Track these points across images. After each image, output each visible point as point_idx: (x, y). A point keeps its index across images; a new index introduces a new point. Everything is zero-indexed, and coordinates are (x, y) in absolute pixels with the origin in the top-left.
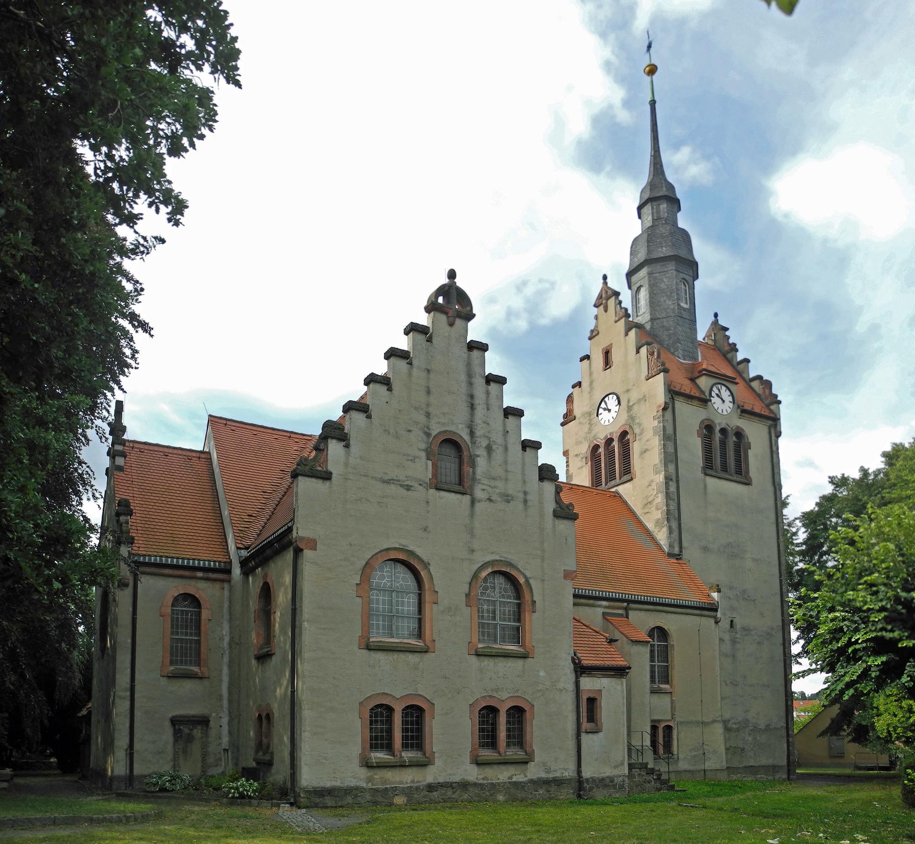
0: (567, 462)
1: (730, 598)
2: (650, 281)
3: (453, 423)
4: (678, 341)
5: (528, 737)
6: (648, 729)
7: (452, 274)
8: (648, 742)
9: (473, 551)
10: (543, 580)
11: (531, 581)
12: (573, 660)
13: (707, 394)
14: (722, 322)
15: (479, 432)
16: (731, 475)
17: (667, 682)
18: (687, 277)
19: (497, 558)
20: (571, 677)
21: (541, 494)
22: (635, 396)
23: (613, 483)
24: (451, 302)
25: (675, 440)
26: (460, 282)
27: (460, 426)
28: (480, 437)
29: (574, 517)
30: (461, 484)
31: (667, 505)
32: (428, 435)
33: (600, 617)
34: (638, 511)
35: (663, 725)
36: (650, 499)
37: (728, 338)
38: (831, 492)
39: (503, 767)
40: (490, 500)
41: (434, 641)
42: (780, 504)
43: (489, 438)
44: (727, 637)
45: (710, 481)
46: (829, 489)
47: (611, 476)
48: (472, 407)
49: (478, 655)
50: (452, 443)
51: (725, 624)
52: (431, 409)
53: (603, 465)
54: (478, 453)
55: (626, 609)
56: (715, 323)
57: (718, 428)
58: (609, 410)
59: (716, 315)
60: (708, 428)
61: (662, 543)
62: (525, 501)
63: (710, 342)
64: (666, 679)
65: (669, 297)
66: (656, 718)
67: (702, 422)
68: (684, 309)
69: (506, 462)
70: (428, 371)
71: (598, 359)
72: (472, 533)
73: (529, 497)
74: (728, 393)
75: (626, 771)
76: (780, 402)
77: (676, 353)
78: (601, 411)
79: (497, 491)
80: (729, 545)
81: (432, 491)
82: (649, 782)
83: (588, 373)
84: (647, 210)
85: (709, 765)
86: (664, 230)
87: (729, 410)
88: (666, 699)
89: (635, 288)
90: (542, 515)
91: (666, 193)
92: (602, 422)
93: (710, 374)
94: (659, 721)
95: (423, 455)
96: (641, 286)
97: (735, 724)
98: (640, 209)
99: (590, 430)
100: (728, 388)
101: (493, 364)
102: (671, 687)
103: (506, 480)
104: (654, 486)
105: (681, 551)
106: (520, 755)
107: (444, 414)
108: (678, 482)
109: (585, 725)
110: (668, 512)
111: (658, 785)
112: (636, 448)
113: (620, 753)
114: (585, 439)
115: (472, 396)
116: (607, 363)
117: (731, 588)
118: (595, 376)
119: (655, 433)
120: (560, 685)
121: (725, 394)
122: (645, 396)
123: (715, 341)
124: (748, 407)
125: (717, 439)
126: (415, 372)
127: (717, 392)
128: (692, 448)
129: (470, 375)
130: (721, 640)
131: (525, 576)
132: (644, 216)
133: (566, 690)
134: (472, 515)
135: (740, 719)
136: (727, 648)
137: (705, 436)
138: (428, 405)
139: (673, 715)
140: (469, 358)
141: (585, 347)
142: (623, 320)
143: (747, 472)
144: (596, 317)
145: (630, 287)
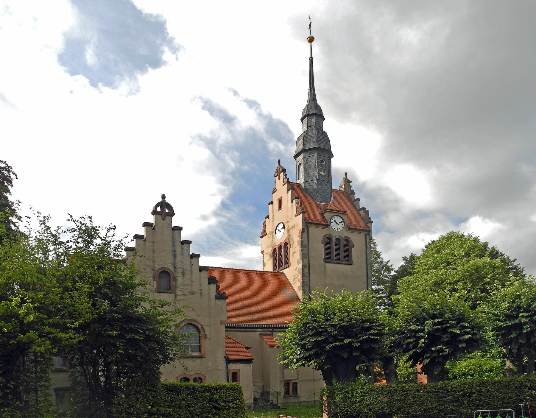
2: (304, 161)
7: (164, 197)
10: (210, 326)
11: (204, 327)
12: (225, 357)
13: (329, 221)
20: (225, 364)
21: (209, 289)
23: (281, 268)
24: (164, 210)
25: (308, 247)
26: (167, 200)
29: (226, 298)
32: (154, 270)
35: (292, 382)
37: (351, 187)
45: (327, 265)
48: (175, 256)
52: (155, 259)
57: (334, 238)
60: (329, 239)
62: (201, 294)
63: (343, 190)
68: (322, 176)
69: (192, 278)
70: (153, 242)
75: (253, 401)
76: (372, 222)
78: (277, 231)
81: (156, 294)
82: (267, 405)
84: (305, 121)
87: (341, 229)
94: (290, 380)
95: (152, 279)
96: (300, 164)
98: (302, 120)
103: (192, 285)
107: (161, 260)
108: (309, 268)
110: (303, 283)
111: (272, 407)
112: (291, 251)
115: (175, 251)
118: (275, 213)
125: (334, 244)
126: (147, 244)
128: (318, 250)
129: (174, 242)
131: (201, 325)
138: (154, 257)
140: (173, 234)
143: (351, 259)
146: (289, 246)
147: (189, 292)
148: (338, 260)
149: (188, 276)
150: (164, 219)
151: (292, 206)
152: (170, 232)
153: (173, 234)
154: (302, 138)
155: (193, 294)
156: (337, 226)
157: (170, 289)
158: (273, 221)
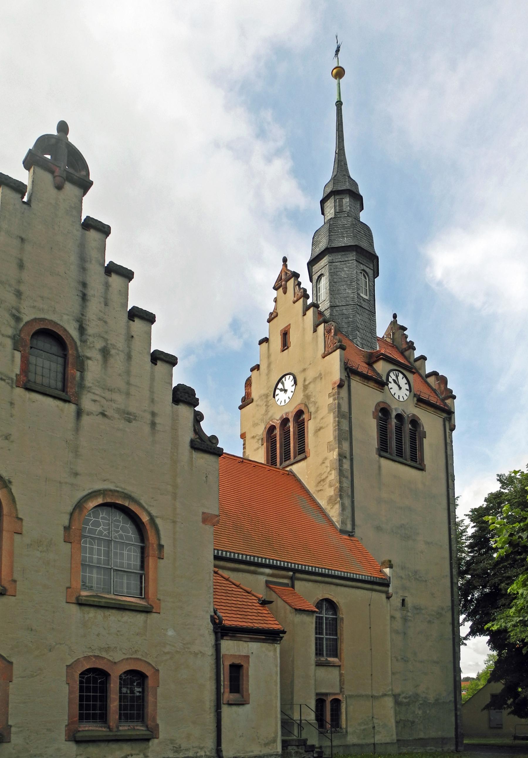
0: (244, 444)
1: (401, 578)
3: (54, 311)
4: (357, 329)
5: (150, 709)
6: (313, 704)
8: (312, 717)
9: (76, 474)
10: (174, 522)
11: (158, 521)
12: (213, 619)
14: (400, 322)
15: (91, 330)
16: (406, 460)
17: (336, 655)
18: (367, 270)
19: (112, 487)
20: (210, 639)
21: (175, 418)
22: (311, 374)
23: (288, 462)
25: (350, 418)
27: (65, 317)
28: (94, 336)
30: (65, 391)
31: (340, 482)
32: (18, 319)
33: (263, 584)
34: (311, 487)
35: (331, 698)
36: (323, 477)
37: (406, 337)
38: (498, 489)
39: (114, 746)
40: (103, 414)
41: (15, 581)
42: (451, 503)
43: (106, 340)
44: (398, 615)
45: (383, 461)
46: (496, 487)
47: (286, 456)
48: (84, 297)
49: (81, 604)
50: (48, 335)
51: (396, 601)
52: (22, 288)
53: (278, 445)
54: (88, 354)
55: (292, 579)
56: (394, 322)
57: (394, 414)
58: (286, 391)
59: (395, 316)
60: (383, 412)
61: (334, 519)
62: (153, 424)
63: (388, 340)
64: (335, 652)
65: (350, 286)
66: (324, 691)
67: (378, 404)
68: (364, 300)
69: (128, 373)
70: (22, 240)
71: (276, 342)
72: (76, 451)
73: (158, 420)
74: (405, 381)
75: (279, 750)
77: (355, 341)
78: (278, 392)
79: (115, 406)
80: (402, 526)
81: (19, 391)
83: (266, 356)
85: (379, 738)
86: (347, 222)
87: (406, 398)
88: (335, 672)
89: (315, 277)
90: (175, 445)
91: (349, 188)
92: (279, 403)
93: (388, 360)
94: (326, 694)
95: (9, 343)
96: (322, 275)
97: (405, 698)
98: (323, 202)
99: (267, 411)
100: (405, 376)
101: (114, 253)
102: (340, 660)
103: (128, 394)
104: (328, 463)
105: (353, 528)
106: (140, 729)
107: (42, 298)
108: (352, 460)
109: (227, 696)
112: (310, 427)
113: (273, 728)
114: (262, 420)
115: (84, 285)
116: (285, 345)
117: (403, 568)
118: (272, 358)
119: (330, 411)
120: (195, 648)
121: (402, 381)
122: (321, 374)
123: (393, 340)
124: (424, 397)
127: (395, 378)
128: (368, 429)
129: (83, 259)
130: (392, 617)
131: (149, 514)
132: (327, 211)
133: (203, 654)
134: (77, 429)
135: (411, 693)
136: (398, 625)
137: (380, 419)
139: (341, 688)
140: (83, 237)
141: (264, 331)
142: (301, 300)
143: (422, 459)
144: (276, 300)
145: (311, 280)
146: (305, 416)
147: (118, 410)
148: (399, 457)
149: (117, 362)
150: (59, 188)
151: (315, 340)
152: (77, 231)
153: (83, 237)
154: (325, 231)
155: (130, 421)
156: (399, 391)
157: (64, 389)
158: (268, 374)
